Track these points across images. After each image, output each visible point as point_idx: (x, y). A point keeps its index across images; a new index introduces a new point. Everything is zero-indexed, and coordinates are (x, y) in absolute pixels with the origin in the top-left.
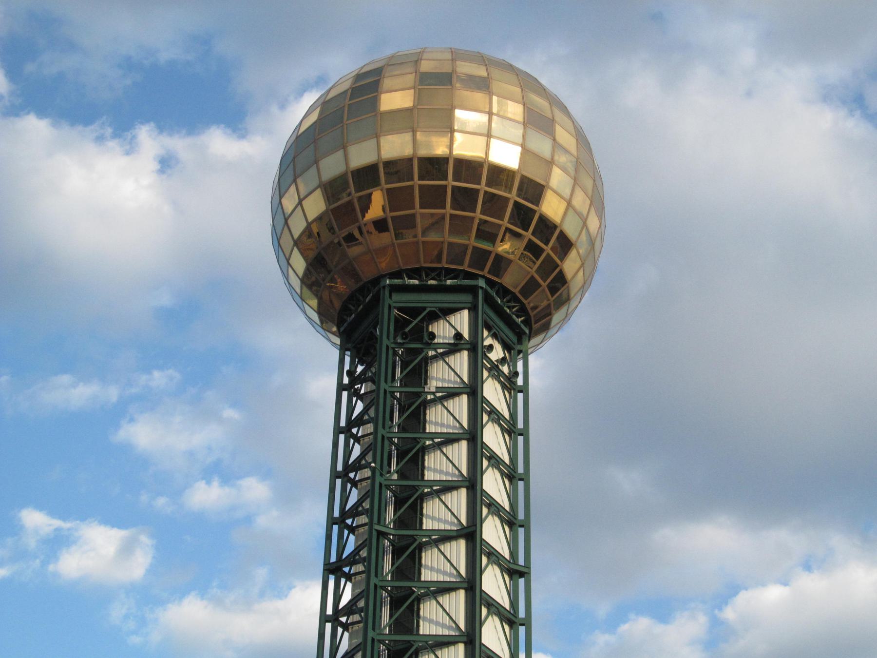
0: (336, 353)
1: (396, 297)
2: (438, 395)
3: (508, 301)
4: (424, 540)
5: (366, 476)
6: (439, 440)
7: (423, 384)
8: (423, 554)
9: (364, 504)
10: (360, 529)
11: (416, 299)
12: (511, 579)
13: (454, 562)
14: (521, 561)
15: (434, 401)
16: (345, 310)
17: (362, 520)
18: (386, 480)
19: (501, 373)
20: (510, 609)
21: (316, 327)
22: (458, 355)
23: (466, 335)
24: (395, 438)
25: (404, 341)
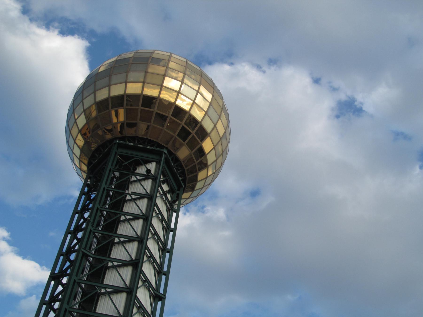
7: (126, 189)
12: (154, 301)
14: (161, 291)
23: (153, 172)
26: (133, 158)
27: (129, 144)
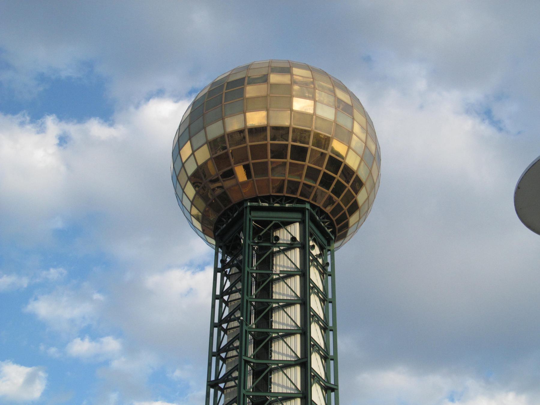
0: (213, 251)
1: (254, 214)
2: (281, 275)
3: (323, 219)
4: (273, 366)
5: (233, 327)
6: (282, 334)
8: (273, 345)
9: (237, 286)
10: (229, 359)
11: (266, 215)
12: (326, 393)
13: (293, 317)
14: (332, 382)
15: (278, 280)
16: (219, 221)
17: (233, 298)
18: (249, 328)
19: (320, 319)
20: (325, 379)
21: (198, 233)
22: (293, 251)
23: (298, 239)
24: (254, 273)
25: (259, 241)
26: (271, 221)
27: (263, 204)
